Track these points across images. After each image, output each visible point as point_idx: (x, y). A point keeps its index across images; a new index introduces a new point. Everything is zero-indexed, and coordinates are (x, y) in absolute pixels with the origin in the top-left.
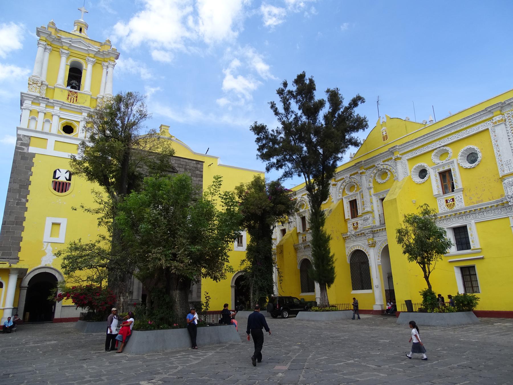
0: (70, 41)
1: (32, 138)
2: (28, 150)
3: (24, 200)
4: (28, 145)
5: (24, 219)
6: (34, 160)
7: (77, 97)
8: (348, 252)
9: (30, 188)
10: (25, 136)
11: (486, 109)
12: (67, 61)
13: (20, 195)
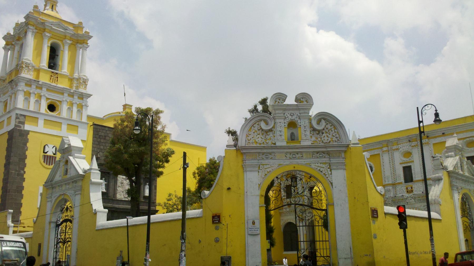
0: (51, 24)
1: (27, 117)
2: (24, 127)
3: (22, 172)
4: (23, 123)
5: (23, 188)
6: (29, 137)
7: (57, 78)
8: (283, 223)
9: (27, 161)
10: (22, 115)
11: (379, 142)
12: (48, 43)
13: (19, 167)
